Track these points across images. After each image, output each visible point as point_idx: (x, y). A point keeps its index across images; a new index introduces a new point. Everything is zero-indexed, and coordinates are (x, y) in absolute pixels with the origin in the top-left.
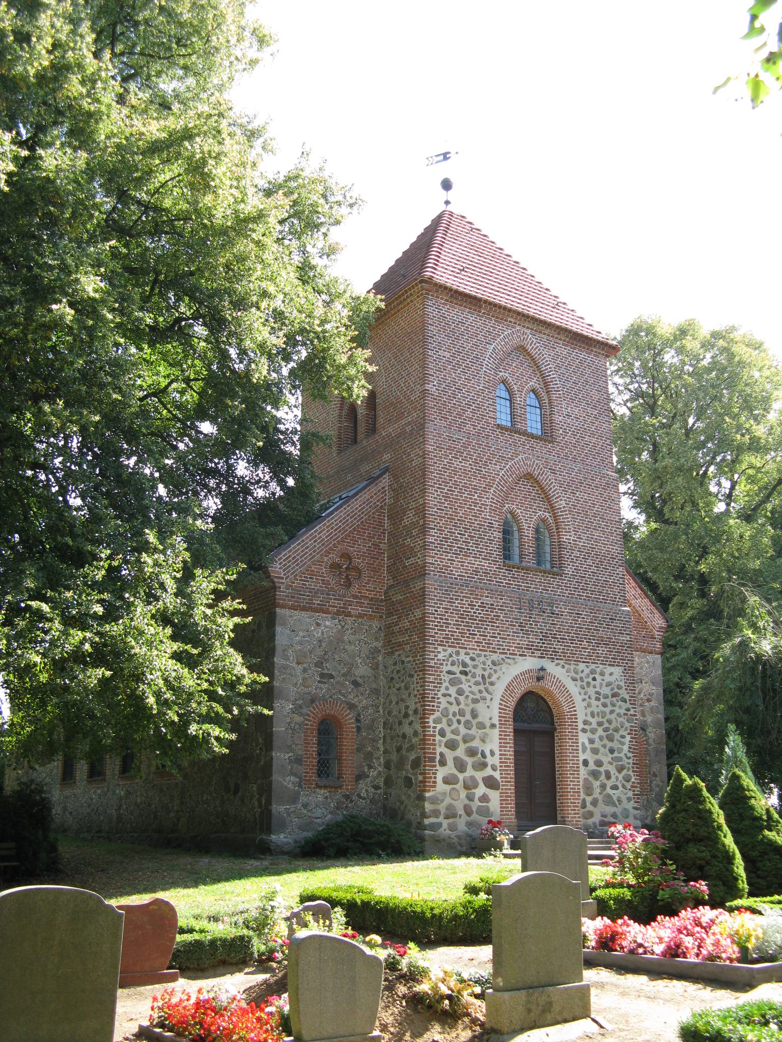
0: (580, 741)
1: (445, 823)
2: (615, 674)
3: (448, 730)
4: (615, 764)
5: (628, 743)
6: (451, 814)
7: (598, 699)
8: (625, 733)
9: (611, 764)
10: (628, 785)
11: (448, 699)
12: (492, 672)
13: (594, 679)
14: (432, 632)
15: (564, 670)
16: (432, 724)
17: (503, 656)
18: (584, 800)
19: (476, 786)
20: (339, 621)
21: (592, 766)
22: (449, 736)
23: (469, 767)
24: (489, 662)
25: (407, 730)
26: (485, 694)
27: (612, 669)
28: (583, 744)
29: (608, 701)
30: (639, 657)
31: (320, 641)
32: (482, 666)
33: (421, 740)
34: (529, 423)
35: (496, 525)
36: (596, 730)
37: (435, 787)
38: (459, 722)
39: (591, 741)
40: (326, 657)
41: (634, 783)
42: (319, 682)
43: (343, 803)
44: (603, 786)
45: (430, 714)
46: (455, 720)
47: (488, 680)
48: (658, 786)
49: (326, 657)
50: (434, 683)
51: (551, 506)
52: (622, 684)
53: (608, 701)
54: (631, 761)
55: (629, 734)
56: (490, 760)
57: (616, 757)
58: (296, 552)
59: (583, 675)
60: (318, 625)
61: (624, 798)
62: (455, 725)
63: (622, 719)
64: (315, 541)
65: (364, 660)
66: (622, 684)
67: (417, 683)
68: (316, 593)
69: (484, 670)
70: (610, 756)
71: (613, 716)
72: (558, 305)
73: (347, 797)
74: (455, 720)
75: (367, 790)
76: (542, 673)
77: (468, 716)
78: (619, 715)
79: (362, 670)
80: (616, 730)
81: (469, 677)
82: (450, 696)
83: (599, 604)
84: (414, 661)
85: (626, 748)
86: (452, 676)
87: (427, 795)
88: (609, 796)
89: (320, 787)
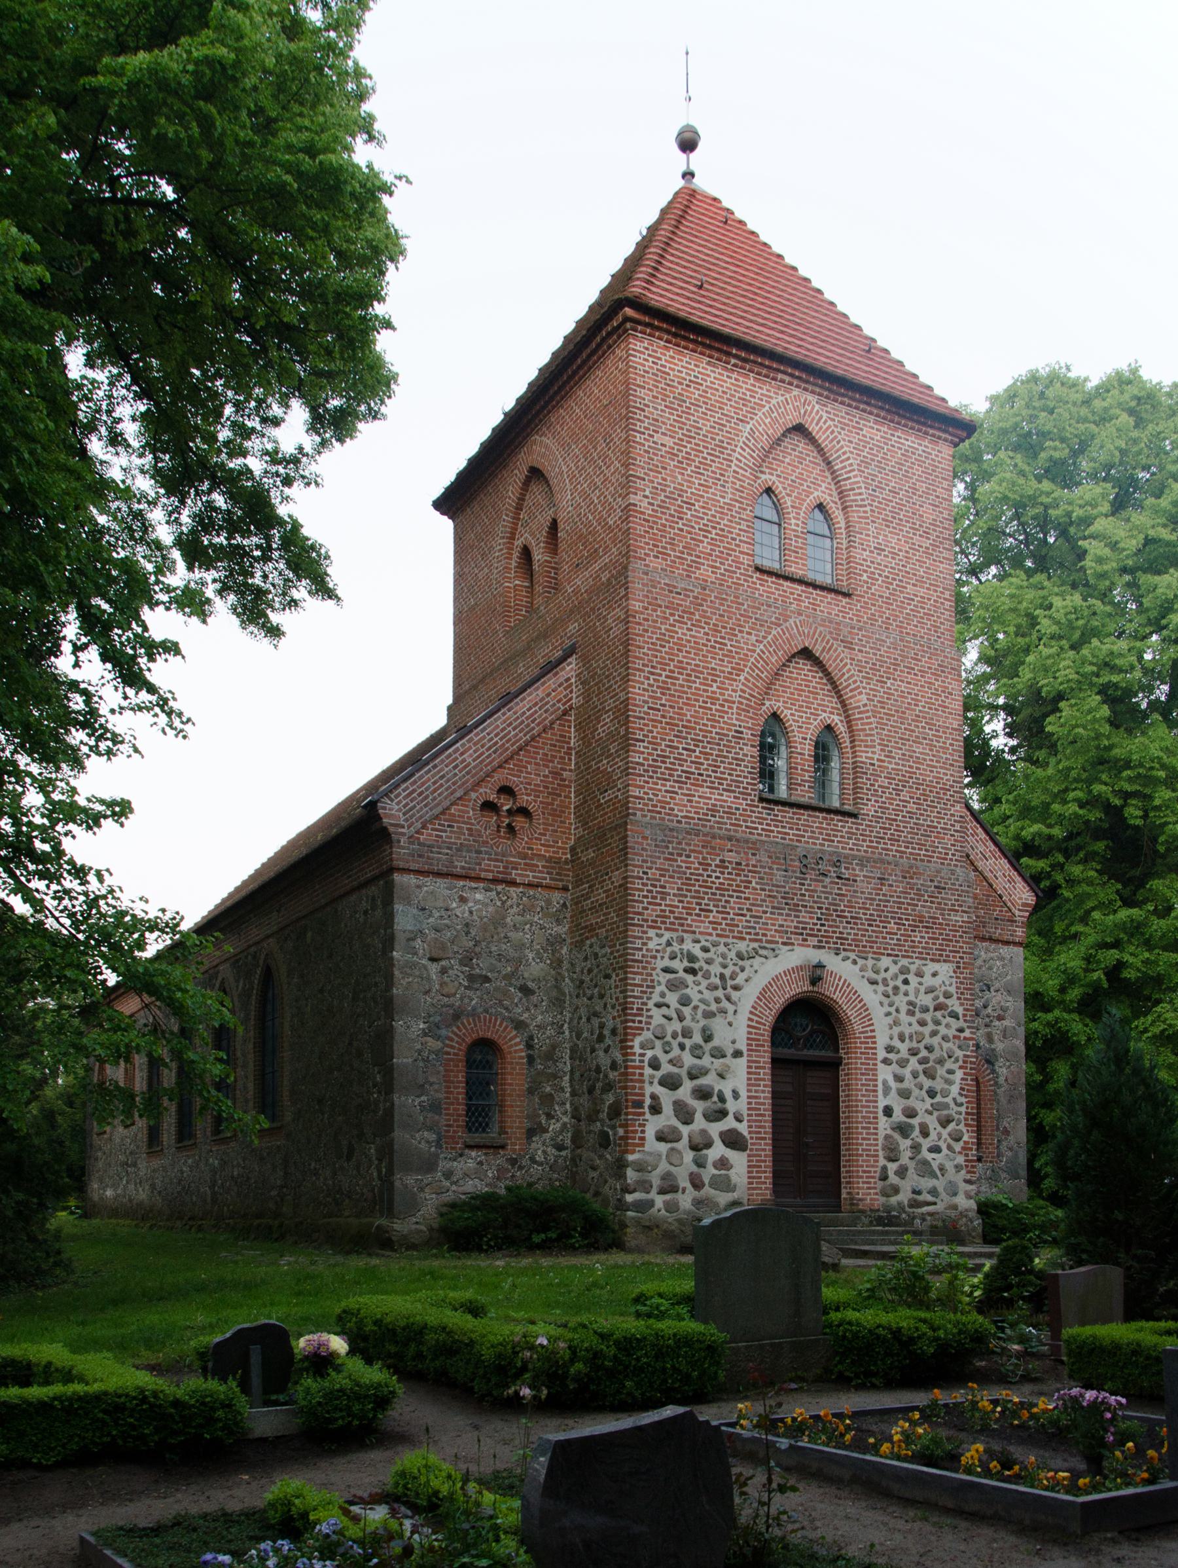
0: (880, 1079)
1: (659, 1201)
2: (942, 974)
3: (663, 1058)
4: (936, 1114)
5: (958, 1081)
6: (669, 1187)
7: (911, 1013)
8: (954, 1067)
9: (930, 1113)
10: (958, 1147)
11: (664, 1010)
12: (737, 969)
13: (906, 982)
14: (639, 907)
15: (857, 968)
16: (637, 1050)
17: (756, 945)
18: (884, 1168)
19: (709, 1145)
20: (498, 893)
21: (898, 1116)
22: (666, 1068)
23: (698, 1116)
24: (732, 955)
25: (604, 1060)
26: (725, 1004)
27: (935, 967)
28: (885, 1082)
29: (928, 1017)
30: (987, 950)
31: (467, 925)
32: (720, 959)
33: (622, 1074)
34: (810, 563)
35: (747, 734)
36: (908, 1061)
37: (643, 1145)
38: (682, 1047)
39: (899, 1079)
40: (477, 949)
41: (965, 1142)
42: (466, 988)
43: (508, 1171)
44: (916, 1148)
45: (635, 1035)
46: (675, 1044)
47: (730, 983)
48: (1011, 1149)
49: (477, 949)
50: (642, 986)
51: (843, 704)
52: (952, 990)
53: (928, 1017)
54: (963, 1109)
55: (961, 1067)
56: (731, 1106)
57: (938, 1103)
58: (423, 784)
59: (888, 975)
60: (463, 900)
61: (949, 1166)
62: (676, 1051)
63: (950, 1045)
64: (455, 767)
65: (538, 953)
66: (952, 990)
67: (616, 987)
68: (458, 850)
69: (725, 967)
70: (929, 1101)
71: (935, 1041)
72: (870, 348)
73: (513, 1162)
74: (675, 1044)
75: (544, 1152)
76: (818, 972)
77: (697, 1038)
78: (945, 1038)
79: (535, 969)
80: (941, 1062)
81: (699, 977)
82: (668, 1007)
83: (919, 863)
84: (612, 953)
85: (955, 1090)
86: (672, 976)
87: (631, 1158)
88: (925, 1163)
89: (471, 1147)
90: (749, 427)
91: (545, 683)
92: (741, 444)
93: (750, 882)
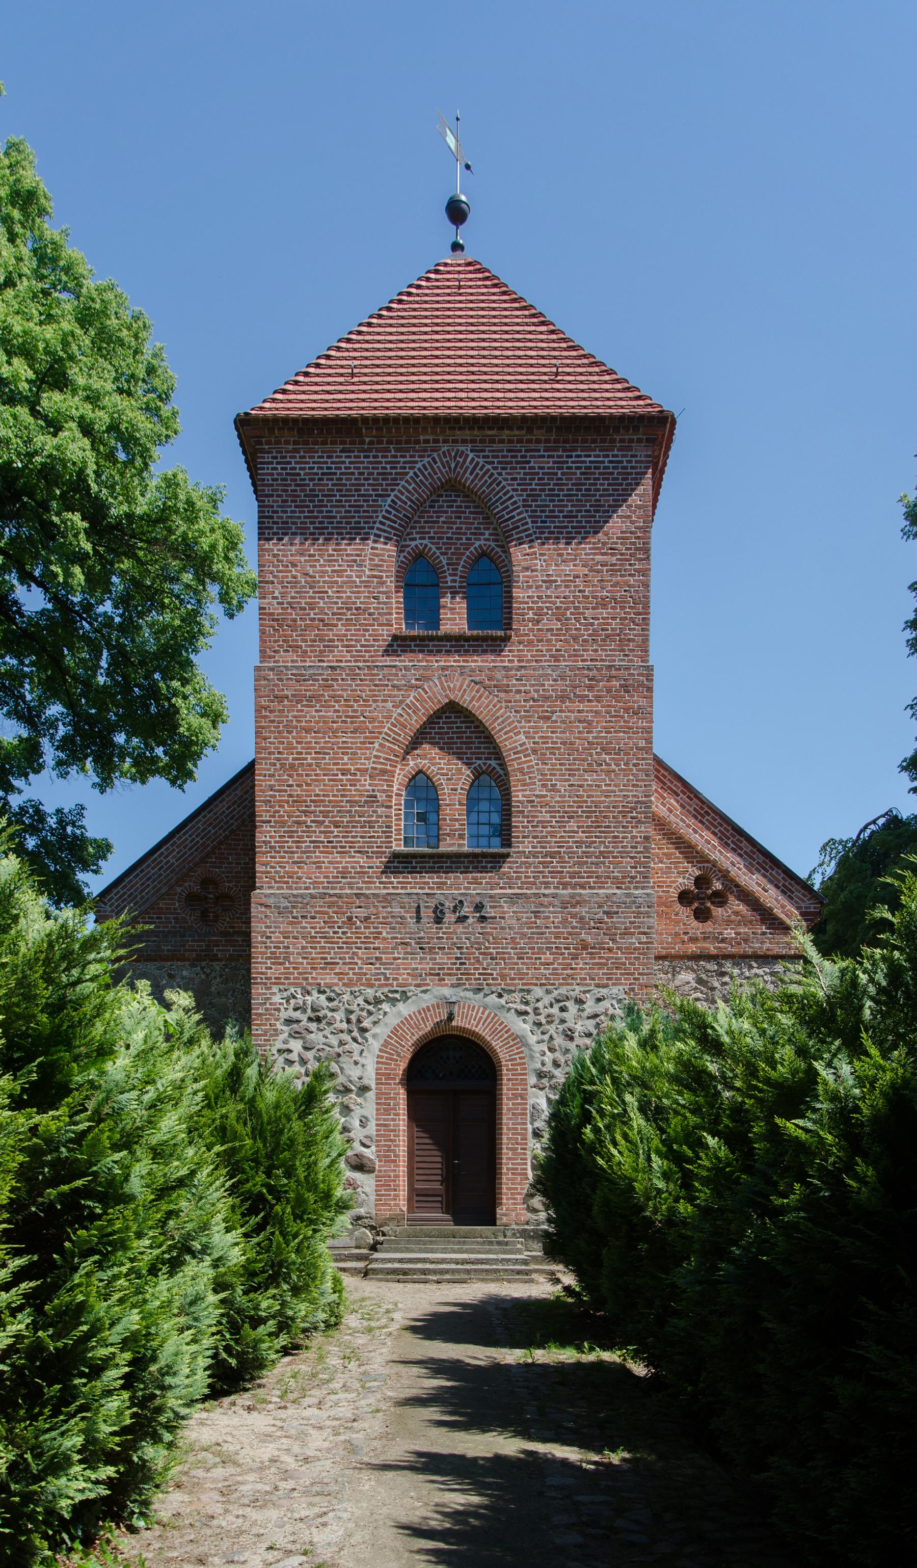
0: (531, 1101)
12: (365, 1014)
17: (386, 990)
20: (202, 968)
58: (132, 887)
64: (160, 869)
90: (389, 499)
91: (243, 782)
92: (380, 519)
93: (381, 933)
